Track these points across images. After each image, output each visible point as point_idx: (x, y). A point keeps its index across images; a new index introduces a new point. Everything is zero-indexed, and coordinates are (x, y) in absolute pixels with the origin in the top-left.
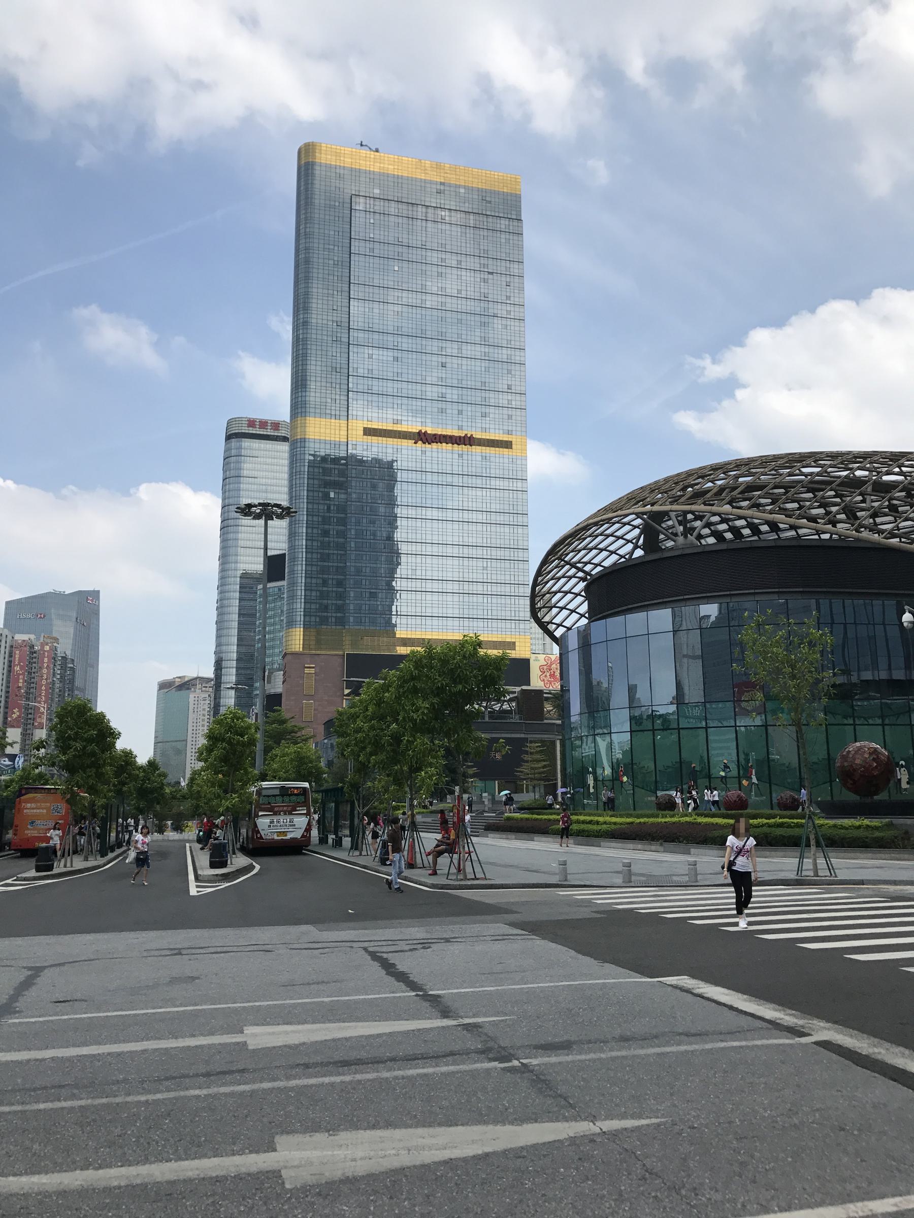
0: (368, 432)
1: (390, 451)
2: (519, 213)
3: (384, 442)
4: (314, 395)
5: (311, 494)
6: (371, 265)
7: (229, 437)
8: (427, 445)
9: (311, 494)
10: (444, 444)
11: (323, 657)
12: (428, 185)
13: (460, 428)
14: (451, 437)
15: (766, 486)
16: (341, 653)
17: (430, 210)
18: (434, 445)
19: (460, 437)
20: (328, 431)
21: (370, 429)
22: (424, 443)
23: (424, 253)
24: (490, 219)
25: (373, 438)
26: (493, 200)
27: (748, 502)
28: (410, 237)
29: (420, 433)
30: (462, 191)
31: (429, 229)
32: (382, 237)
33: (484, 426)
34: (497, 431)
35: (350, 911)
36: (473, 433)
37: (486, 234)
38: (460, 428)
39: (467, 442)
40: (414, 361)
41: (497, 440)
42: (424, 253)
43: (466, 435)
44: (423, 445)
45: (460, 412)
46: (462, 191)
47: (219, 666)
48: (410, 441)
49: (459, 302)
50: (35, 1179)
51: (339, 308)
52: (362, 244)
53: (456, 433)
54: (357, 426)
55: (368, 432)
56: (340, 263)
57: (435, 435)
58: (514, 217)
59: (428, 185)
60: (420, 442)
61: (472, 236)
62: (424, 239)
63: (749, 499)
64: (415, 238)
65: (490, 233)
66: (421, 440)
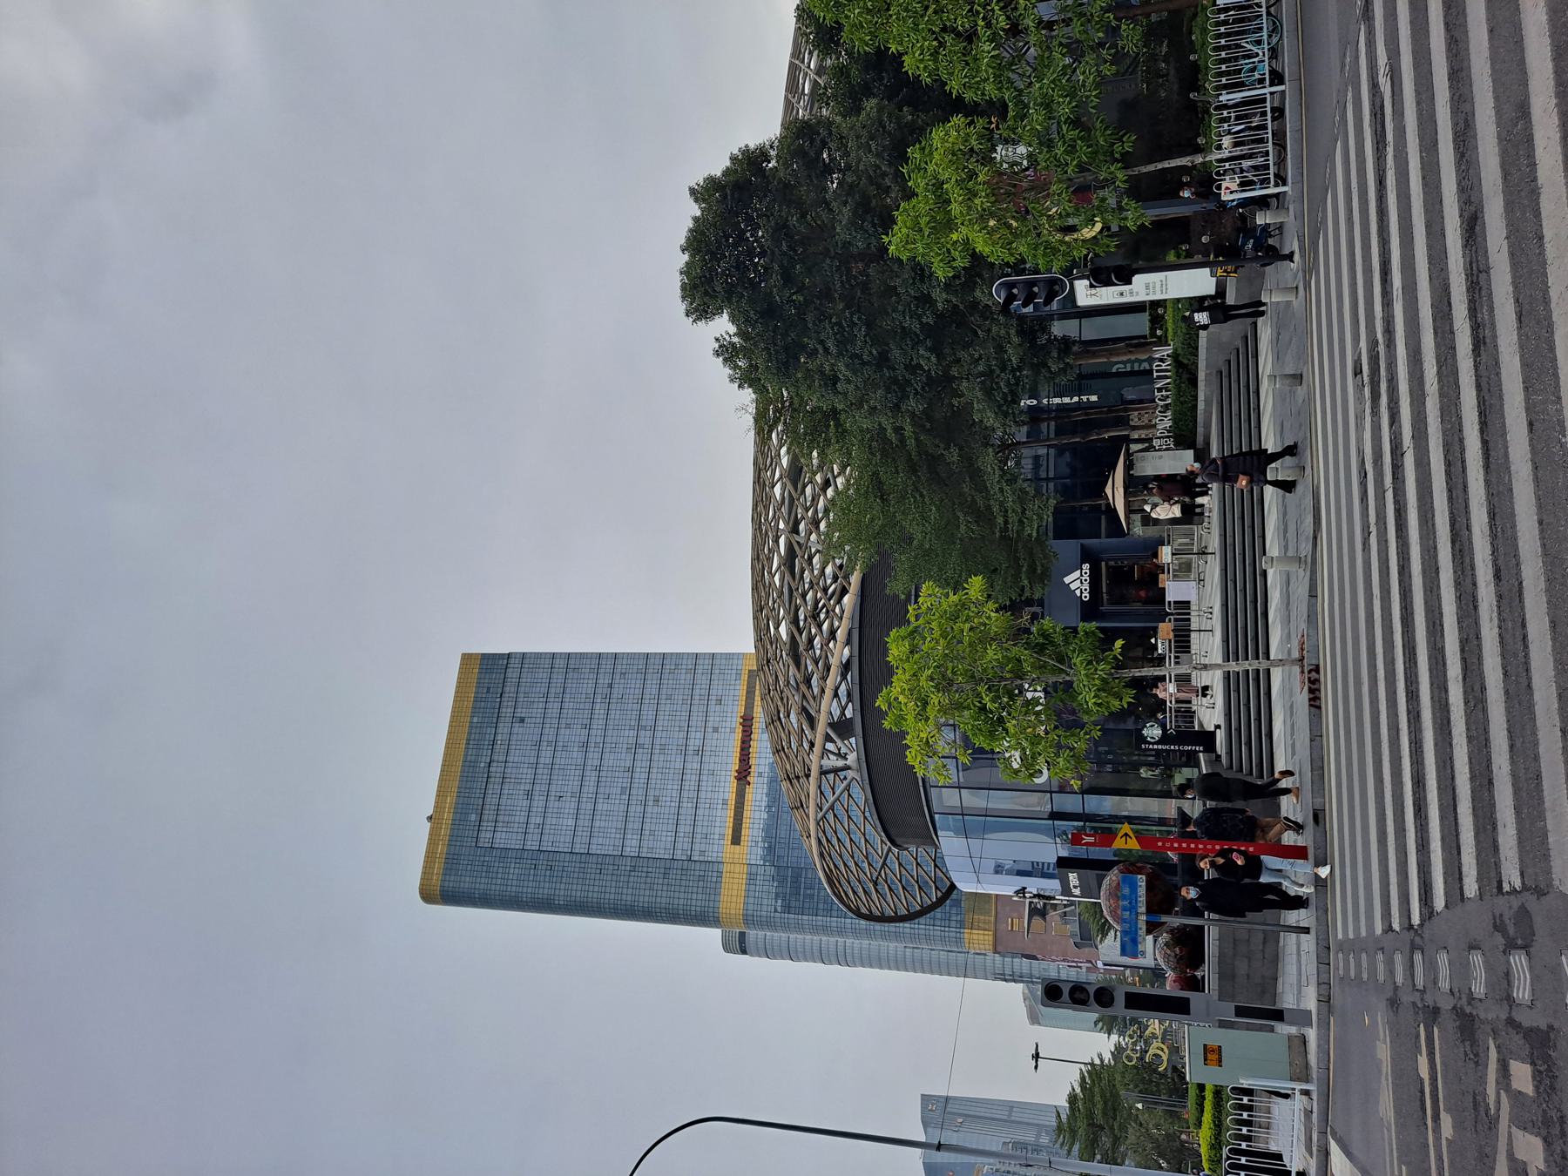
0: (736, 840)
1: (757, 815)
2: (501, 656)
3: (748, 821)
4: (697, 903)
5: (806, 911)
6: (553, 827)
7: (744, 952)
8: (752, 770)
9: (806, 911)
10: (751, 750)
12: (469, 758)
13: (733, 731)
14: (743, 742)
15: (791, 543)
17: (495, 758)
18: (752, 761)
19: (744, 731)
20: (735, 887)
21: (733, 838)
22: (749, 773)
23: (542, 766)
24: (507, 689)
25: (745, 815)
26: (486, 685)
27: (806, 572)
28: (523, 781)
29: (738, 779)
30: (475, 720)
31: (516, 759)
32: (523, 813)
33: (720, 806)
34: (737, 687)
35: (1094, 398)
36: (739, 715)
37: (522, 695)
38: (733, 731)
39: (748, 723)
40: (671, 682)
41: (736, 802)
42: (542, 766)
43: (736, 777)
44: (752, 774)
45: (716, 730)
46: (475, 720)
47: (1014, 978)
48: (747, 790)
49: (595, 727)
50: (1435, 792)
51: (599, 867)
52: (529, 837)
53: (738, 735)
54: (728, 851)
55: (736, 840)
56: (550, 863)
57: (740, 761)
58: (505, 661)
59: (469, 758)
60: (748, 778)
61: (524, 710)
62: (530, 743)
63: (802, 571)
64: (524, 776)
65: (522, 689)
66: (746, 777)
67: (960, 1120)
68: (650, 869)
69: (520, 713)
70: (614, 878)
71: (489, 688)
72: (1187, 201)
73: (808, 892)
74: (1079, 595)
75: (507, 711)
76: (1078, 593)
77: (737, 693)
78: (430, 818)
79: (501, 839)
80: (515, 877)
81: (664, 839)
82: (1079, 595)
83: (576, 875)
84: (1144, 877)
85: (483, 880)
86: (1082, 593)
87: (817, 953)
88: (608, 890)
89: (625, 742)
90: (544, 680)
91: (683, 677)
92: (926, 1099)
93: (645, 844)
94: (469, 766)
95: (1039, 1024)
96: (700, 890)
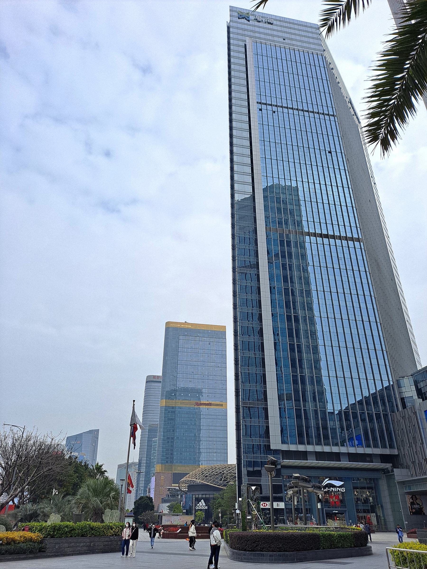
11: (166, 473)
16: (171, 472)
30: (210, 331)
46: (210, 331)
58: (224, 338)
67: (94, 445)
68: (174, 381)
69: (211, 343)
70: (172, 372)
71: (217, 334)
72: (273, 517)
73: (169, 423)
74: (197, 505)
75: (212, 340)
76: (198, 505)
77: (217, 401)
78: (186, 322)
79: (181, 342)
80: (172, 346)
81: (181, 384)
82: (197, 505)
83: (173, 362)
84: (262, 503)
85: (171, 338)
86: (198, 506)
87: (147, 395)
88: (169, 370)
89: (205, 372)
90: (208, 390)
91: (221, 386)
92: (98, 431)
93: (180, 379)
94: (198, 331)
95: (118, 468)
96: (170, 367)
